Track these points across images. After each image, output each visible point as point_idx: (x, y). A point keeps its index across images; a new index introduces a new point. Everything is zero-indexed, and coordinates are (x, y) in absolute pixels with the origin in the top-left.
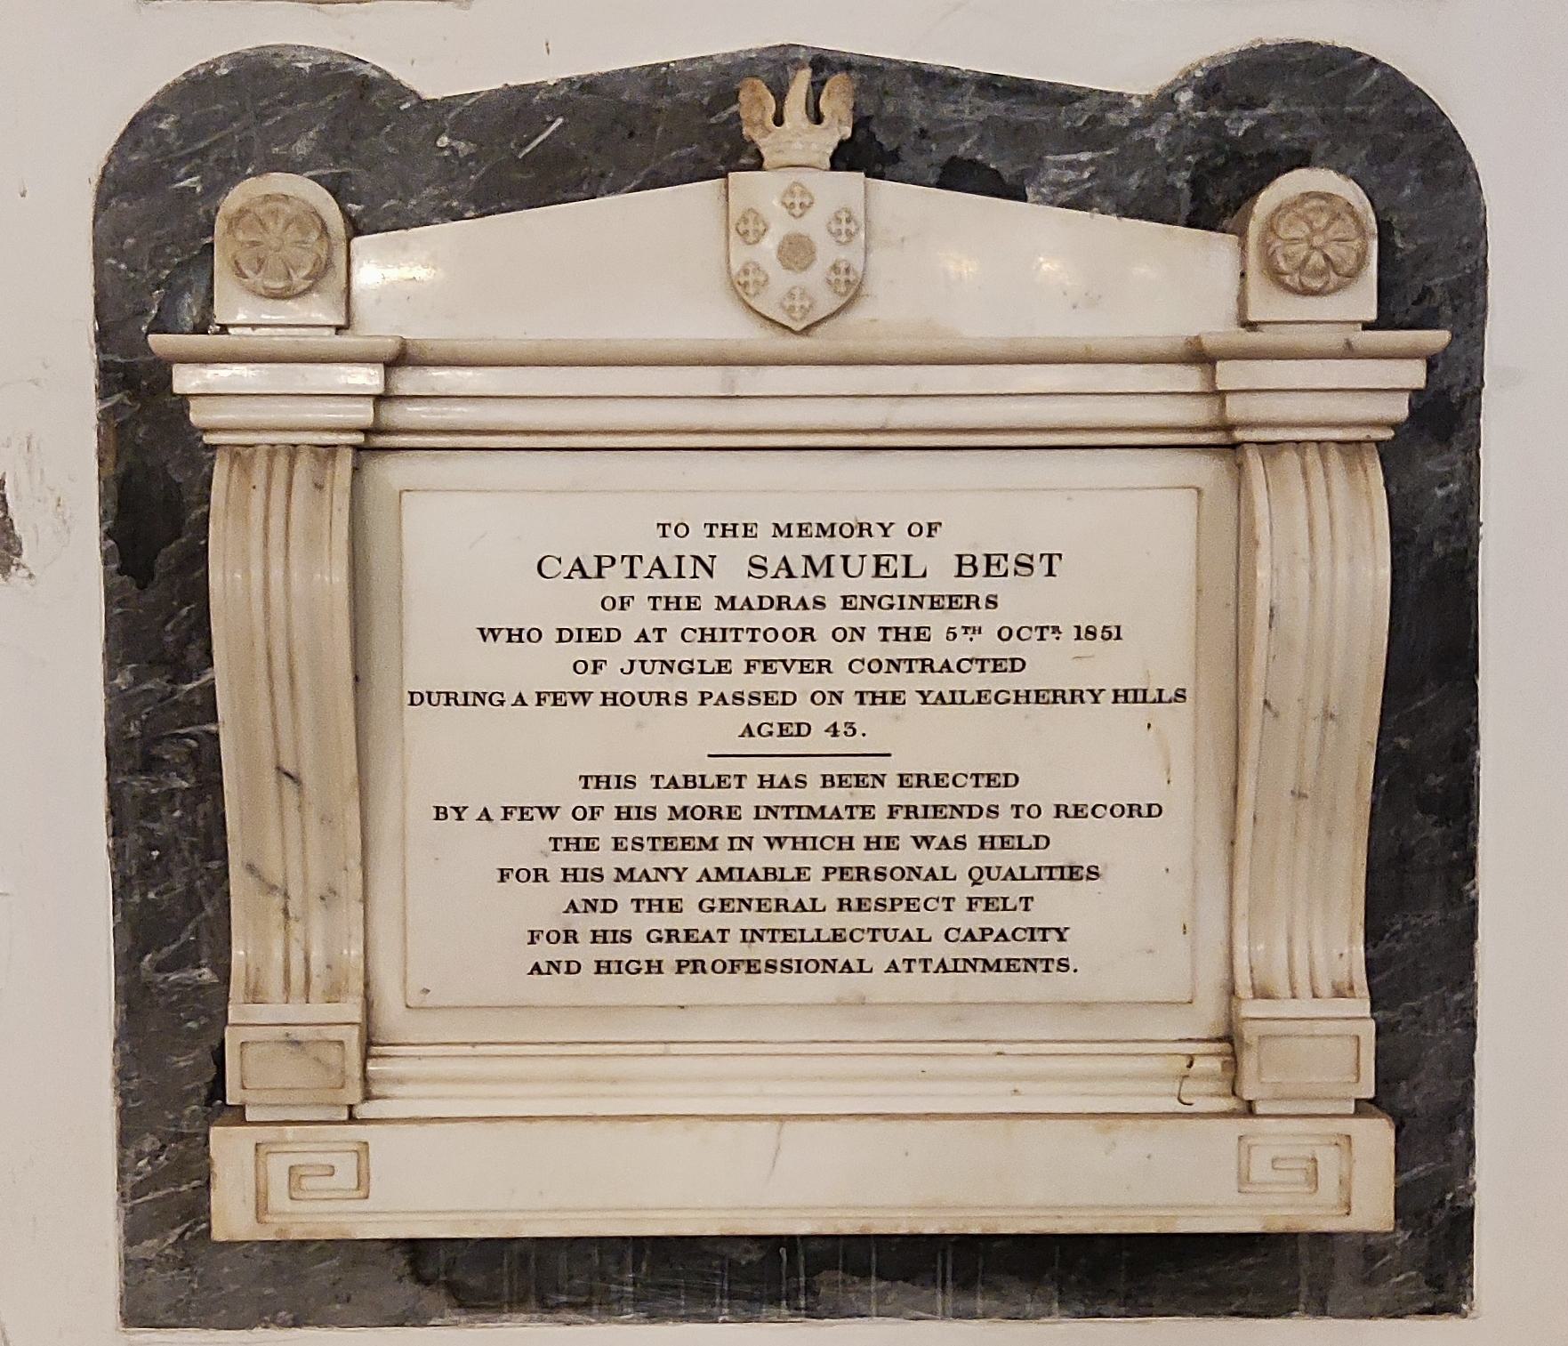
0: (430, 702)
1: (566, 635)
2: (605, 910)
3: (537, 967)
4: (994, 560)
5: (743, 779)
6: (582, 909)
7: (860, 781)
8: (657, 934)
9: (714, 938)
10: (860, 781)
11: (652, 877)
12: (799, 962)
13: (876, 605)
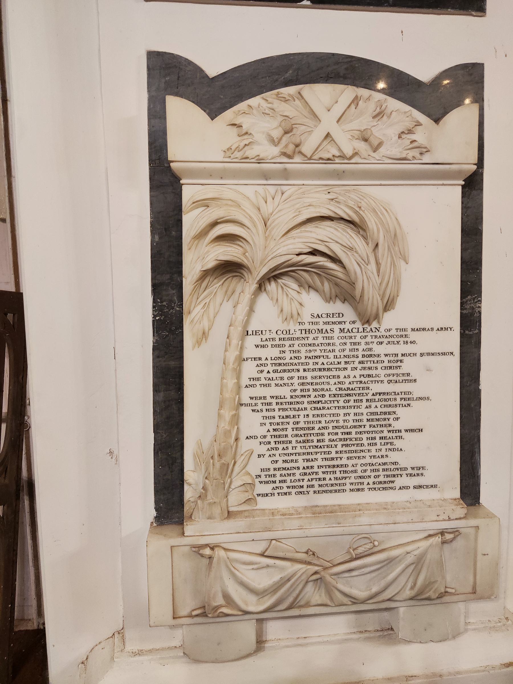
0: (343, 428)
1: (357, 433)
2: (339, 428)
3: (270, 455)
4: (257, 332)
5: (299, 416)
6: (270, 450)
7: (390, 367)
8: (302, 474)
9: (322, 447)
10: (390, 367)
11: (248, 387)
12: (445, 353)
13: (281, 429)
